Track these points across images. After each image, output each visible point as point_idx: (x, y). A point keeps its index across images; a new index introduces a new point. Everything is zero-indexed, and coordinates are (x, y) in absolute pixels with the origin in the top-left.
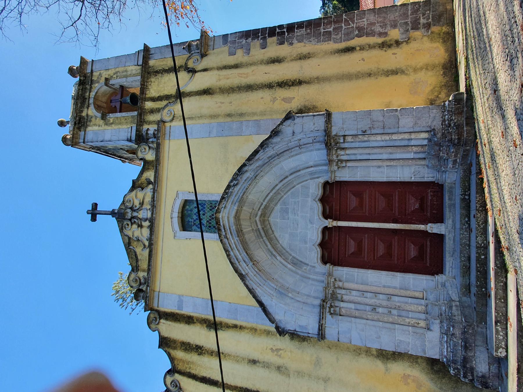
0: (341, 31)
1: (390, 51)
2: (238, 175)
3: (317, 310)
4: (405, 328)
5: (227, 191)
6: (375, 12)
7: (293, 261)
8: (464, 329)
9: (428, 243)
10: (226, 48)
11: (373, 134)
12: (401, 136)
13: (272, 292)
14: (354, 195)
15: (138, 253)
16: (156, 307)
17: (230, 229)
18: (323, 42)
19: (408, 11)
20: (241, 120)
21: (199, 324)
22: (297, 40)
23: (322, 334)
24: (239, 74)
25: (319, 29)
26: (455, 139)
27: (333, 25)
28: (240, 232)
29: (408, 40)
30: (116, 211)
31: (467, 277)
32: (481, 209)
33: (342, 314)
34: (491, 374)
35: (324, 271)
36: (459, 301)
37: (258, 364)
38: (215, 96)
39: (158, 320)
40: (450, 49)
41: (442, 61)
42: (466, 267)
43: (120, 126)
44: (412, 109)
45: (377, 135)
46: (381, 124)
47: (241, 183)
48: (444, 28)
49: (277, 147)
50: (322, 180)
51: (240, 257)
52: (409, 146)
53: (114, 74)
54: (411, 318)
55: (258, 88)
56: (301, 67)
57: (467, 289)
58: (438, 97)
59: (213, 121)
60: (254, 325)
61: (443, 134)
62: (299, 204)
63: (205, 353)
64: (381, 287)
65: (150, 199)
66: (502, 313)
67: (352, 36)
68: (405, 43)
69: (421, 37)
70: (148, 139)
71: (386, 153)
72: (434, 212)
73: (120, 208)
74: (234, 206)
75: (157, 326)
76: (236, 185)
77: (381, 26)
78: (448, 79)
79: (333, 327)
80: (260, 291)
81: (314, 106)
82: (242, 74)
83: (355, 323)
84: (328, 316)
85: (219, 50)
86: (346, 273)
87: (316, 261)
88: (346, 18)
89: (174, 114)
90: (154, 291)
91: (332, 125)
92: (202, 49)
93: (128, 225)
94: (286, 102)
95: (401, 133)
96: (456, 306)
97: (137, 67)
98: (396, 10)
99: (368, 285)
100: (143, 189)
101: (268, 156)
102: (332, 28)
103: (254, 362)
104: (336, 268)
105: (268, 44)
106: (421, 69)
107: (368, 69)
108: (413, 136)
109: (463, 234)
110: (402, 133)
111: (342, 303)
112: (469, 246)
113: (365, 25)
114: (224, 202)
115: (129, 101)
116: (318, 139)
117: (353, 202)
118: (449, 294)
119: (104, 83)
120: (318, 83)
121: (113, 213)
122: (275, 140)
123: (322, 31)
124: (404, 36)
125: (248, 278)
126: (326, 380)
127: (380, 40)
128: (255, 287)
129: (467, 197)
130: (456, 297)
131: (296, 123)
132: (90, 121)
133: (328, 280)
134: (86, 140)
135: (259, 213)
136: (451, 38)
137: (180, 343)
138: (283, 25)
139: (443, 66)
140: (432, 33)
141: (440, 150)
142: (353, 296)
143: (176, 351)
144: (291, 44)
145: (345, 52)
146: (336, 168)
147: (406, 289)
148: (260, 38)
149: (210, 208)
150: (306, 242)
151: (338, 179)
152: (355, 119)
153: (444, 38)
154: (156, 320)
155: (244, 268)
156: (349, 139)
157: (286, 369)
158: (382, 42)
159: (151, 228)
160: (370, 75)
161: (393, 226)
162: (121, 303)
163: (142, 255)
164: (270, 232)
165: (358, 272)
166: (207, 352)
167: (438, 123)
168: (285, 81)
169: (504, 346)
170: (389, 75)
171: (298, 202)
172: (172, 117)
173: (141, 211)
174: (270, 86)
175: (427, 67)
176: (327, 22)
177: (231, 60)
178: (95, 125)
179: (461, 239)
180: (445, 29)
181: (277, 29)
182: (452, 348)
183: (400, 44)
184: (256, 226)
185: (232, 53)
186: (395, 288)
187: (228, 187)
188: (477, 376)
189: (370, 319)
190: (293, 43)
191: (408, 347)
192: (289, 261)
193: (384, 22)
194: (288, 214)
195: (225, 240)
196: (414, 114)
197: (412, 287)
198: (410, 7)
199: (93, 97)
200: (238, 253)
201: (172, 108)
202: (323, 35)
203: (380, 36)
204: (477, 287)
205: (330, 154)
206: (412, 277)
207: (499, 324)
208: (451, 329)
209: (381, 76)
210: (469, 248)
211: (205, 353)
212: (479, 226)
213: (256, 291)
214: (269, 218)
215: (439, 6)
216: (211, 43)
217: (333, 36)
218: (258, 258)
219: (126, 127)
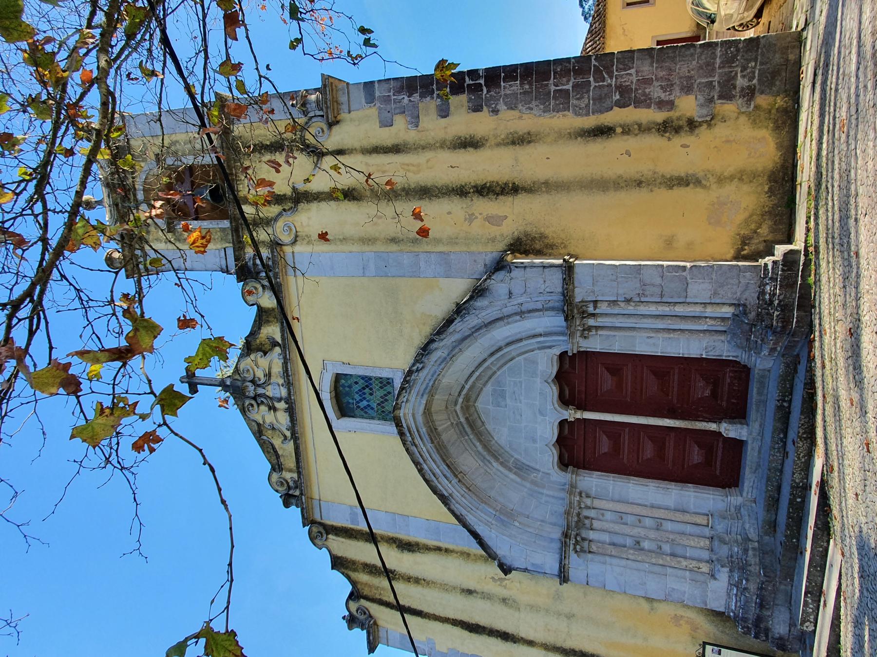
0: (588, 92)
1: (678, 141)
2: (423, 355)
3: (556, 546)
4: (680, 573)
5: (408, 378)
6: (652, 57)
7: (516, 464)
8: (762, 585)
10: (372, 112)
13: (490, 520)
14: (608, 369)
15: (277, 447)
16: (318, 519)
17: (418, 431)
18: (553, 111)
19: (715, 59)
21: (385, 544)
22: (506, 104)
23: (564, 576)
24: (403, 164)
25: (547, 85)
26: (777, 327)
27: (572, 78)
28: (433, 432)
29: (712, 119)
31: (773, 512)
32: (805, 436)
34: (791, 637)
35: (563, 481)
36: (758, 542)
37: (475, 594)
38: (364, 204)
39: (325, 536)
40: (786, 143)
41: (770, 165)
42: (773, 499)
44: (711, 270)
45: (650, 305)
46: (658, 290)
47: (430, 367)
48: (779, 100)
49: (483, 314)
50: (557, 351)
51: (438, 470)
55: (440, 195)
56: (516, 160)
57: (772, 526)
58: (755, 232)
59: (366, 248)
60: (466, 549)
61: (758, 315)
62: (521, 386)
63: (399, 578)
66: (816, 584)
67: (608, 103)
68: (705, 126)
69: (736, 114)
72: (733, 401)
74: (421, 398)
75: (325, 543)
76: (421, 369)
77: (662, 87)
78: (776, 202)
79: (580, 568)
80: (473, 518)
81: (541, 234)
82: (408, 165)
83: (611, 564)
84: (573, 556)
85: (360, 113)
86: (596, 485)
88: (597, 64)
89: (296, 232)
90: (312, 499)
91: (576, 285)
92: (329, 113)
93: (252, 405)
95: (689, 303)
96: (754, 549)
98: (692, 55)
100: (265, 353)
101: (469, 327)
102: (571, 84)
103: (470, 592)
105: (452, 108)
106: (731, 178)
107: (637, 172)
109: (773, 456)
111: (591, 532)
112: (781, 471)
113: (632, 82)
114: (404, 393)
116: (551, 304)
117: (607, 382)
118: (745, 529)
120: (547, 192)
122: (480, 303)
123: (553, 88)
124: (704, 111)
125: (453, 501)
126: (570, 616)
127: (659, 116)
128: (464, 512)
129: (785, 404)
130: (754, 535)
131: (514, 277)
133: (570, 499)
135: (460, 400)
136: (789, 122)
138: (477, 70)
139: (769, 177)
140: (755, 107)
141: (751, 332)
142: (607, 521)
143: (357, 573)
144: (495, 112)
145: (595, 135)
147: (684, 511)
148: (435, 95)
150: (534, 441)
152: (614, 277)
153: (777, 120)
154: (322, 534)
155: (448, 486)
156: (603, 308)
157: (514, 601)
158: (664, 121)
159: (291, 411)
160: (639, 184)
161: (669, 423)
163: (284, 450)
164: (479, 423)
166: (402, 577)
167: (753, 295)
168: (488, 185)
169: (812, 620)
170: (673, 186)
171: (521, 382)
172: (293, 236)
173: (270, 386)
174: (461, 192)
175: (742, 176)
176: (561, 70)
177: (386, 136)
179: (769, 462)
180: (780, 102)
181: (467, 79)
182: (742, 603)
183: (696, 127)
184: (456, 418)
185: (387, 123)
186: (667, 509)
188: (772, 637)
190: (498, 111)
191: (684, 596)
192: (510, 464)
193: (669, 80)
194: (505, 399)
195: (413, 448)
196: (714, 277)
197: (692, 506)
198: (718, 51)
200: (434, 465)
201: (290, 219)
202: (555, 98)
203: (660, 108)
204: (786, 536)
205: (571, 326)
207: (809, 595)
208: (744, 582)
209: (659, 188)
210: (781, 475)
211: (399, 578)
212: (799, 458)
214: (475, 402)
215: (775, 52)
216: (343, 99)
217: (573, 101)
218: (465, 468)
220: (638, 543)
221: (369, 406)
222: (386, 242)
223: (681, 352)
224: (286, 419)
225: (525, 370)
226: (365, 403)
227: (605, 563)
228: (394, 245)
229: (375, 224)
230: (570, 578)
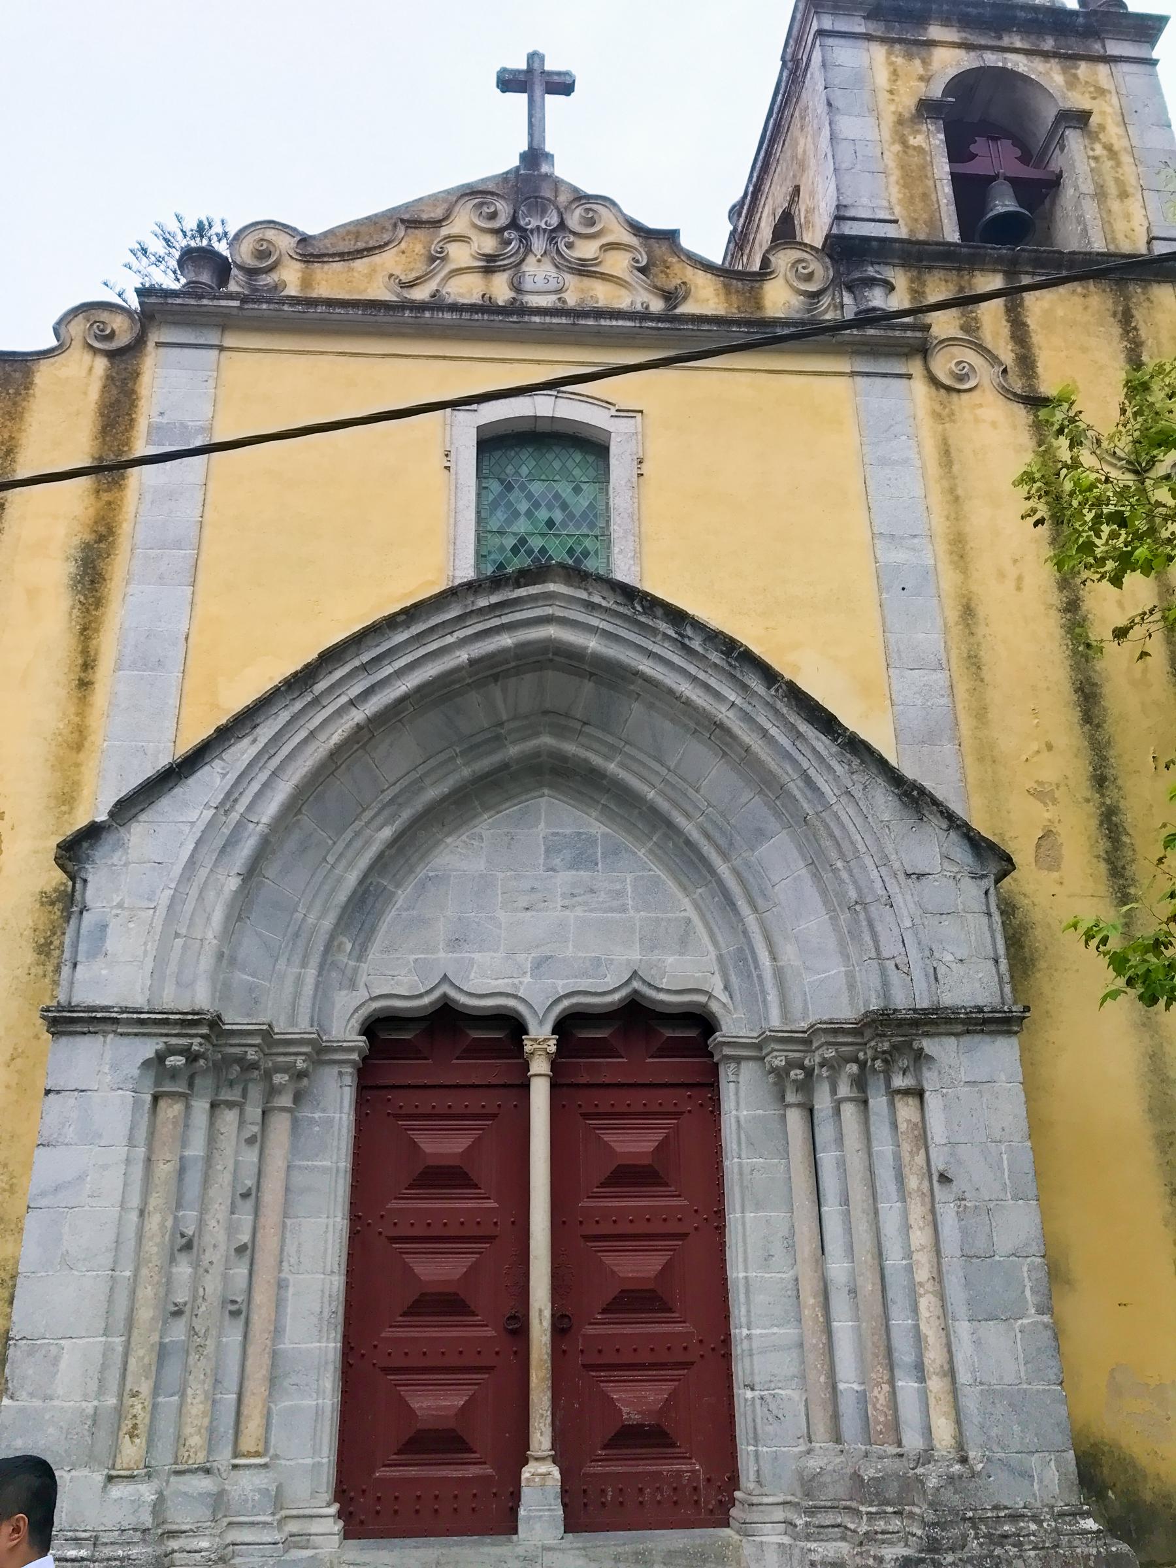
9: (472, 1471)
11: (933, 1211)
12: (931, 1332)
15: (377, 259)
16: (154, 337)
30: (545, 169)
33: (162, 1104)
43: (895, 175)
45: (929, 1230)
52: (892, 1370)
53: (1109, 148)
54: (155, 1406)
59: (942, 547)
62: (612, 910)
64: (280, 1271)
65: (602, 303)
70: (850, 289)
71: (853, 1274)
73: (557, 183)
75: (77, 344)
80: (247, 758)
87: (378, 992)
89: (959, 391)
94: (1038, 846)
97: (1145, 239)
99: (286, 1215)
104: (349, 1080)
108: (936, 1384)
110: (948, 1336)
115: (1000, 209)
119: (1068, 105)
121: (534, 156)
122: (883, 801)
132: (909, 56)
134: (830, 41)
137: (11, 438)
142: (237, 1153)
146: (780, 1062)
147: (273, 1381)
149: (579, 550)
150: (455, 943)
151: (726, 1073)
156: (907, 1111)
162: (150, 250)
165: (338, 1170)
171: (623, 909)
172: (948, 382)
178: (895, 75)
186: (277, 1331)
187: (677, 616)
189: (147, 1228)
199: (1009, 66)
206: (328, 1402)
213: (246, 741)
219: (894, 201)
220: (188, 1246)
221: (516, 514)
222: (964, 596)
223: (756, 1332)
224: (461, 295)
225: (658, 920)
226: (523, 507)
227: (131, 1143)
228: (957, 614)
229: (1001, 575)
230: (64, 1040)
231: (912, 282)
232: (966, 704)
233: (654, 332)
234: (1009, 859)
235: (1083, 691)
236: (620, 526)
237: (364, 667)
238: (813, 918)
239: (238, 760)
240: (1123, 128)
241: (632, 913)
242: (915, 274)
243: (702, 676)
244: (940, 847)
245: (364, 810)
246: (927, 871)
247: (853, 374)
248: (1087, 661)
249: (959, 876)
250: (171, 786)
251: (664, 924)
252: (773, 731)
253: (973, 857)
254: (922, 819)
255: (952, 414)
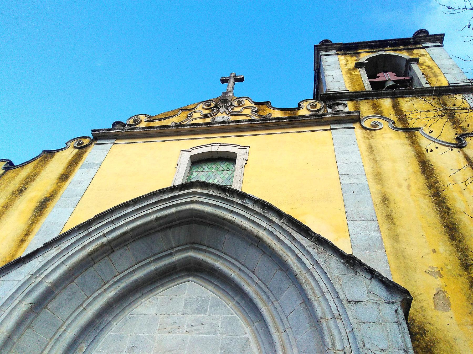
20: (380, 219)
62: (210, 333)
94: (435, 298)
171: (215, 333)
231: (354, 104)
232: (387, 234)
233: (257, 125)
234: (407, 292)
235: (448, 227)
236: (236, 179)
237: (112, 222)
238: (304, 332)
239: (49, 256)
240: (433, 61)
241: (219, 335)
242: (355, 102)
243: (252, 218)
244: (368, 287)
245: (105, 284)
246: (360, 299)
247: (330, 129)
248: (448, 215)
249: (378, 302)
250: (18, 267)
251: (235, 340)
252: (283, 238)
253: (386, 292)
254: (356, 274)
255: (372, 136)
